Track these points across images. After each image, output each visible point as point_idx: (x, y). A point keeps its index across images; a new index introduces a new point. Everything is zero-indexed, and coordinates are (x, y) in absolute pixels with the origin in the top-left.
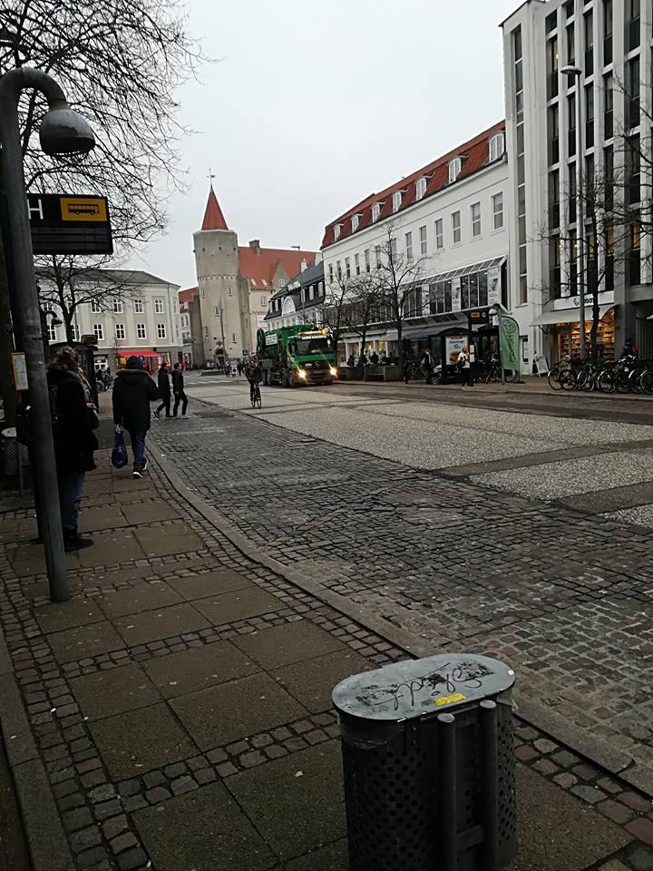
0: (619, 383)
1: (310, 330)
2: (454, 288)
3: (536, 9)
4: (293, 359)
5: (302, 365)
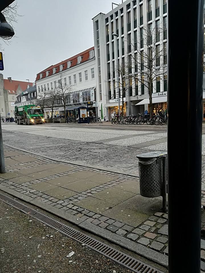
0: (130, 122)
1: (34, 106)
2: (80, 95)
3: (103, 16)
4: (29, 116)
5: (32, 117)
